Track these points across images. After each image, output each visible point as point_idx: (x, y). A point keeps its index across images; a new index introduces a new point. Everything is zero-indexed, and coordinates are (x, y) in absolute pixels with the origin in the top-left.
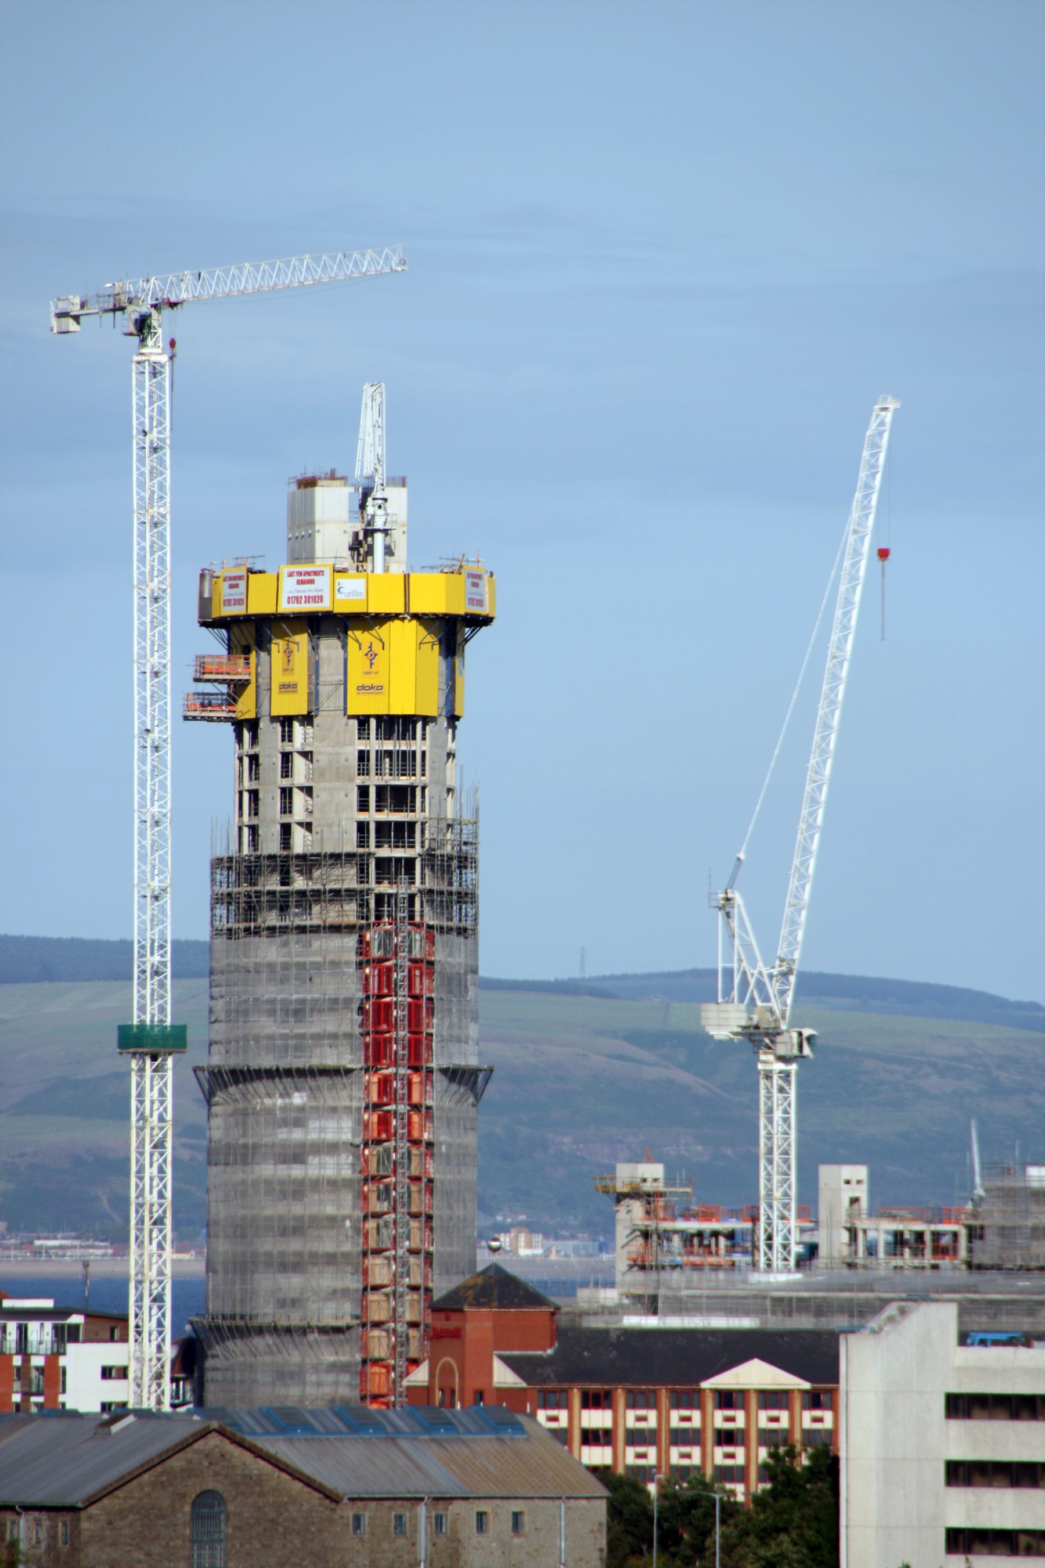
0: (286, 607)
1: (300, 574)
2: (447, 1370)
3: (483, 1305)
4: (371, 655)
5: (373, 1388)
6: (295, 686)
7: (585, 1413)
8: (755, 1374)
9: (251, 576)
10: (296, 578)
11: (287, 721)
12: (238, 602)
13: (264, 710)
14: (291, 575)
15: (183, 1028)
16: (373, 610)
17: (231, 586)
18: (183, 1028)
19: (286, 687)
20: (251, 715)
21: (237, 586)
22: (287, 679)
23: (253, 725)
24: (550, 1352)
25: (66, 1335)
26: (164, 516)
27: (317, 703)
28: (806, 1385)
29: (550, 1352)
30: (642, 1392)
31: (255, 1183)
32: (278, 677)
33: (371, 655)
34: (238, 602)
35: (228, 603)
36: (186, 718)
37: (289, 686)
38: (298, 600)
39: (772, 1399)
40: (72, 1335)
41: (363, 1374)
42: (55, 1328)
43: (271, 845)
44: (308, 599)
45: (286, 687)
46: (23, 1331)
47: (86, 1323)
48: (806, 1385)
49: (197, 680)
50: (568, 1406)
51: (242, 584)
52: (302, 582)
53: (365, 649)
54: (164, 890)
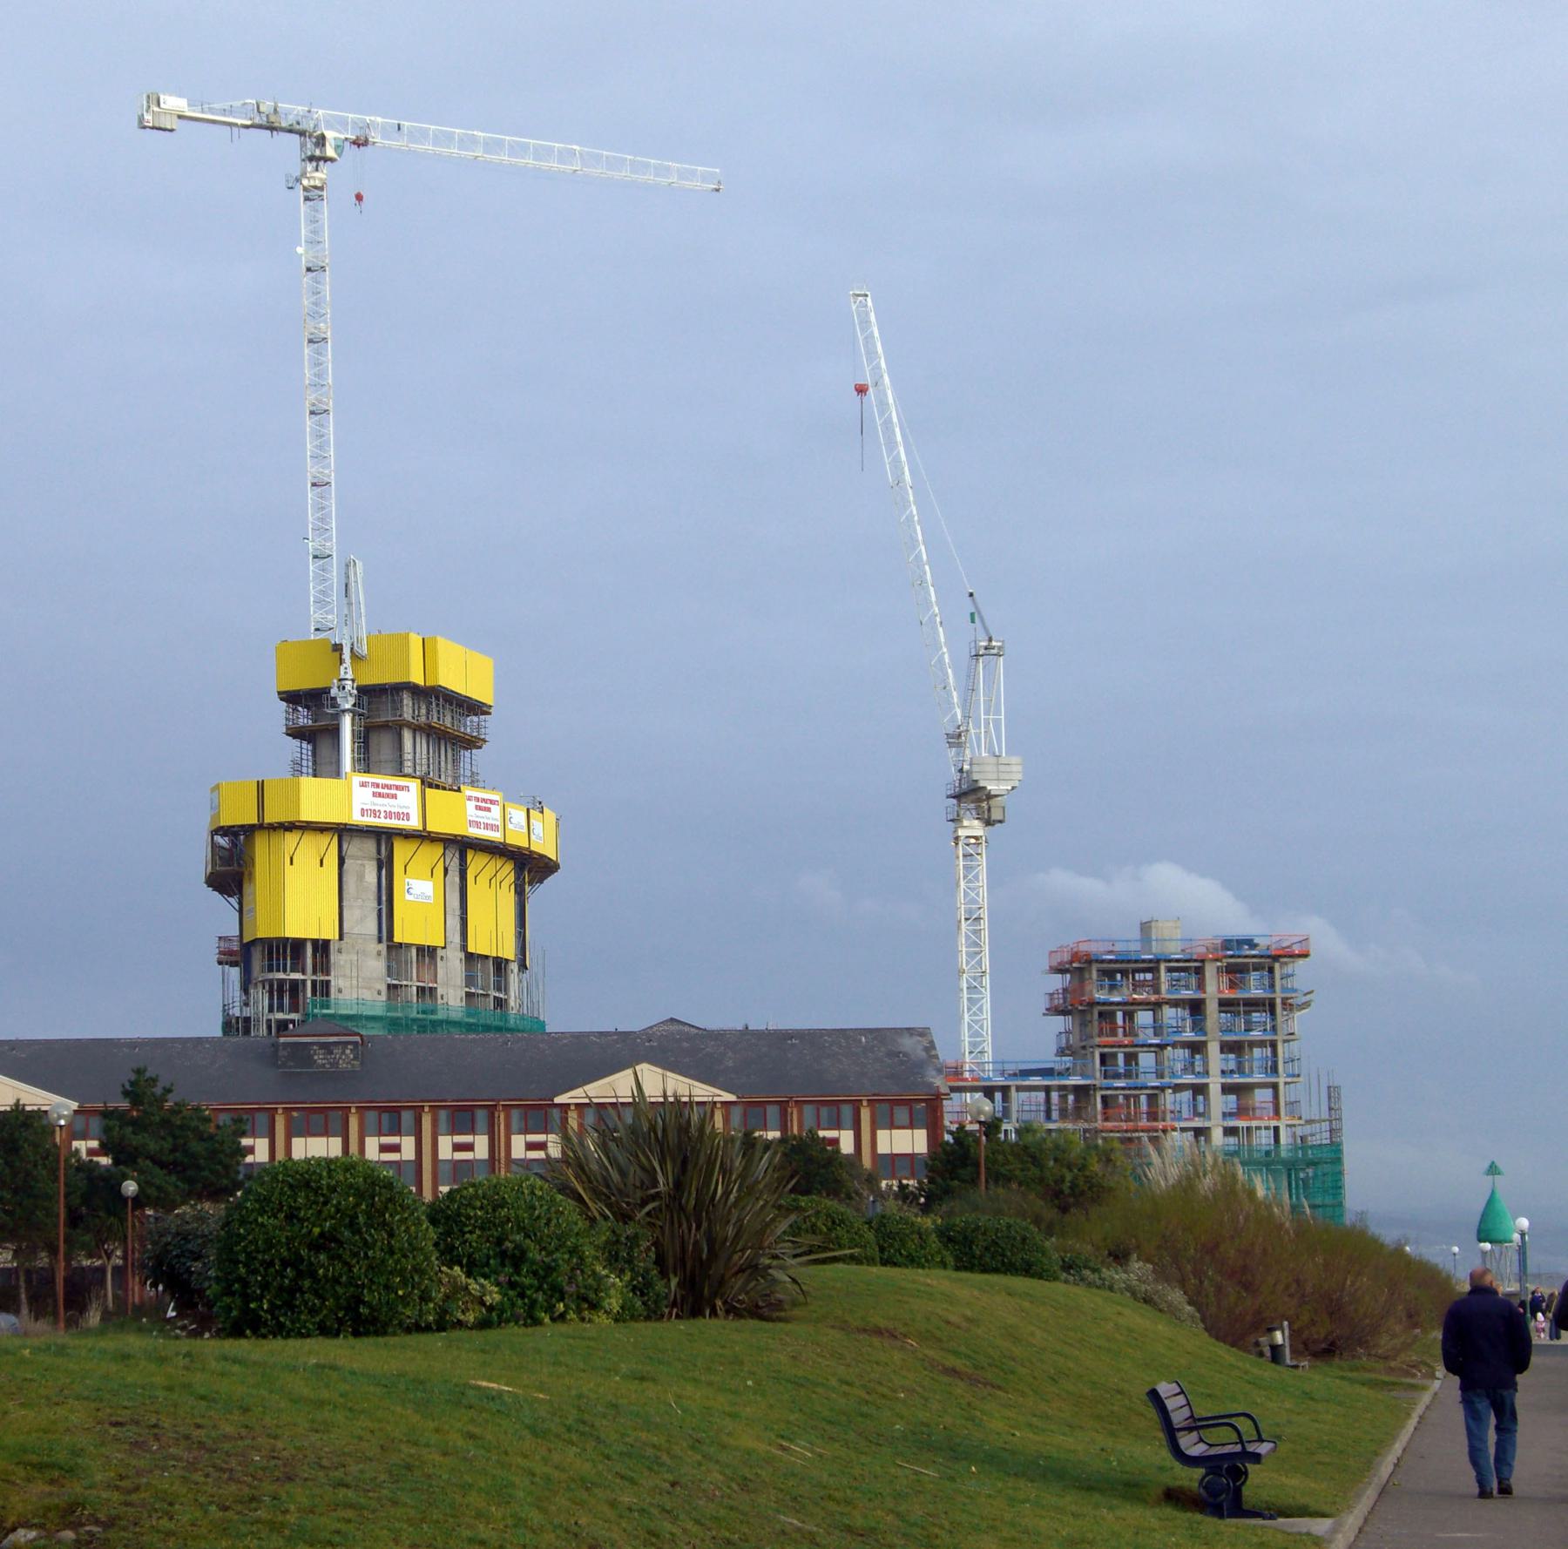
1: (477, 799)
10: (370, 790)
12: (494, 828)
14: (363, 785)
17: (479, 808)
34: (494, 828)
38: (375, 813)
44: (389, 815)
51: (496, 811)
52: (380, 795)
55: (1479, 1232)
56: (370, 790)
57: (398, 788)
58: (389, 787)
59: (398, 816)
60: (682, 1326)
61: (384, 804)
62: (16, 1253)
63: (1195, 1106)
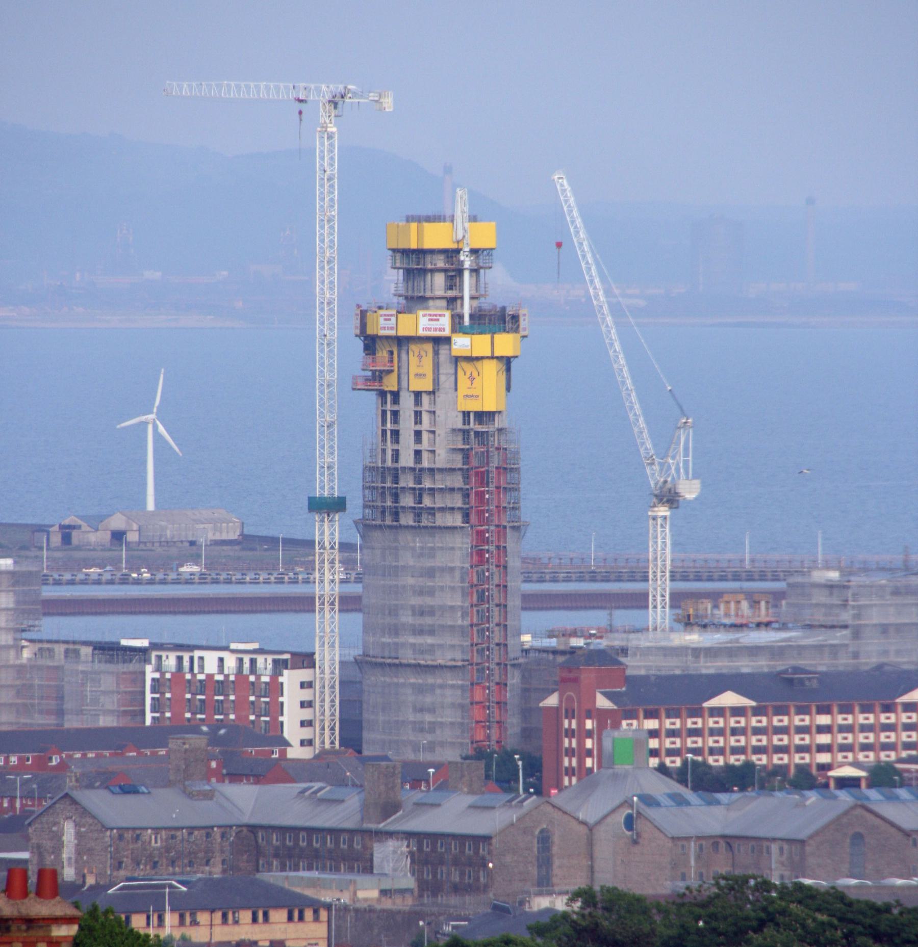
0: (421, 333)
1: (430, 315)
2: (570, 699)
3: (590, 665)
4: (472, 379)
5: (477, 698)
6: (425, 375)
7: (646, 721)
8: (729, 699)
9: (399, 315)
10: (427, 318)
11: (418, 395)
12: (391, 328)
13: (404, 384)
14: (424, 315)
15: (344, 498)
16: (475, 354)
17: (386, 320)
18: (344, 498)
19: (418, 375)
20: (395, 389)
21: (390, 320)
22: (421, 371)
23: (396, 396)
24: (624, 689)
25: (280, 666)
26: (334, 216)
27: (438, 384)
28: (754, 704)
29: (624, 689)
30: (673, 709)
31: (404, 587)
32: (413, 370)
33: (472, 379)
34: (391, 328)
35: (384, 328)
36: (354, 389)
37: (421, 375)
38: (429, 329)
39: (738, 711)
40: (284, 664)
41: (472, 690)
42: (274, 661)
43: (407, 460)
44: (435, 330)
45: (418, 375)
46: (253, 662)
47: (292, 658)
48: (754, 704)
49: (363, 370)
50: (637, 718)
51: (393, 319)
52: (432, 320)
53: (468, 375)
54: (333, 422)
55: (506, 592)
56: (427, 318)
57: (440, 315)
58: (435, 315)
59: (440, 330)
60: (243, 937)
61: (434, 324)
62: (15, 562)
63: (865, 569)
